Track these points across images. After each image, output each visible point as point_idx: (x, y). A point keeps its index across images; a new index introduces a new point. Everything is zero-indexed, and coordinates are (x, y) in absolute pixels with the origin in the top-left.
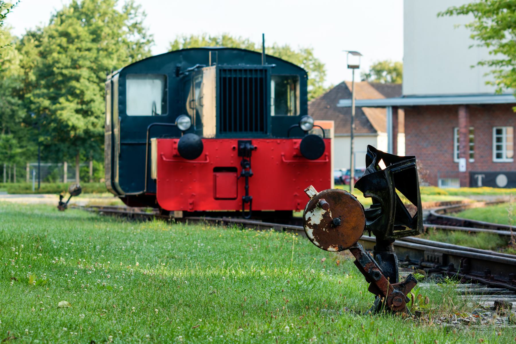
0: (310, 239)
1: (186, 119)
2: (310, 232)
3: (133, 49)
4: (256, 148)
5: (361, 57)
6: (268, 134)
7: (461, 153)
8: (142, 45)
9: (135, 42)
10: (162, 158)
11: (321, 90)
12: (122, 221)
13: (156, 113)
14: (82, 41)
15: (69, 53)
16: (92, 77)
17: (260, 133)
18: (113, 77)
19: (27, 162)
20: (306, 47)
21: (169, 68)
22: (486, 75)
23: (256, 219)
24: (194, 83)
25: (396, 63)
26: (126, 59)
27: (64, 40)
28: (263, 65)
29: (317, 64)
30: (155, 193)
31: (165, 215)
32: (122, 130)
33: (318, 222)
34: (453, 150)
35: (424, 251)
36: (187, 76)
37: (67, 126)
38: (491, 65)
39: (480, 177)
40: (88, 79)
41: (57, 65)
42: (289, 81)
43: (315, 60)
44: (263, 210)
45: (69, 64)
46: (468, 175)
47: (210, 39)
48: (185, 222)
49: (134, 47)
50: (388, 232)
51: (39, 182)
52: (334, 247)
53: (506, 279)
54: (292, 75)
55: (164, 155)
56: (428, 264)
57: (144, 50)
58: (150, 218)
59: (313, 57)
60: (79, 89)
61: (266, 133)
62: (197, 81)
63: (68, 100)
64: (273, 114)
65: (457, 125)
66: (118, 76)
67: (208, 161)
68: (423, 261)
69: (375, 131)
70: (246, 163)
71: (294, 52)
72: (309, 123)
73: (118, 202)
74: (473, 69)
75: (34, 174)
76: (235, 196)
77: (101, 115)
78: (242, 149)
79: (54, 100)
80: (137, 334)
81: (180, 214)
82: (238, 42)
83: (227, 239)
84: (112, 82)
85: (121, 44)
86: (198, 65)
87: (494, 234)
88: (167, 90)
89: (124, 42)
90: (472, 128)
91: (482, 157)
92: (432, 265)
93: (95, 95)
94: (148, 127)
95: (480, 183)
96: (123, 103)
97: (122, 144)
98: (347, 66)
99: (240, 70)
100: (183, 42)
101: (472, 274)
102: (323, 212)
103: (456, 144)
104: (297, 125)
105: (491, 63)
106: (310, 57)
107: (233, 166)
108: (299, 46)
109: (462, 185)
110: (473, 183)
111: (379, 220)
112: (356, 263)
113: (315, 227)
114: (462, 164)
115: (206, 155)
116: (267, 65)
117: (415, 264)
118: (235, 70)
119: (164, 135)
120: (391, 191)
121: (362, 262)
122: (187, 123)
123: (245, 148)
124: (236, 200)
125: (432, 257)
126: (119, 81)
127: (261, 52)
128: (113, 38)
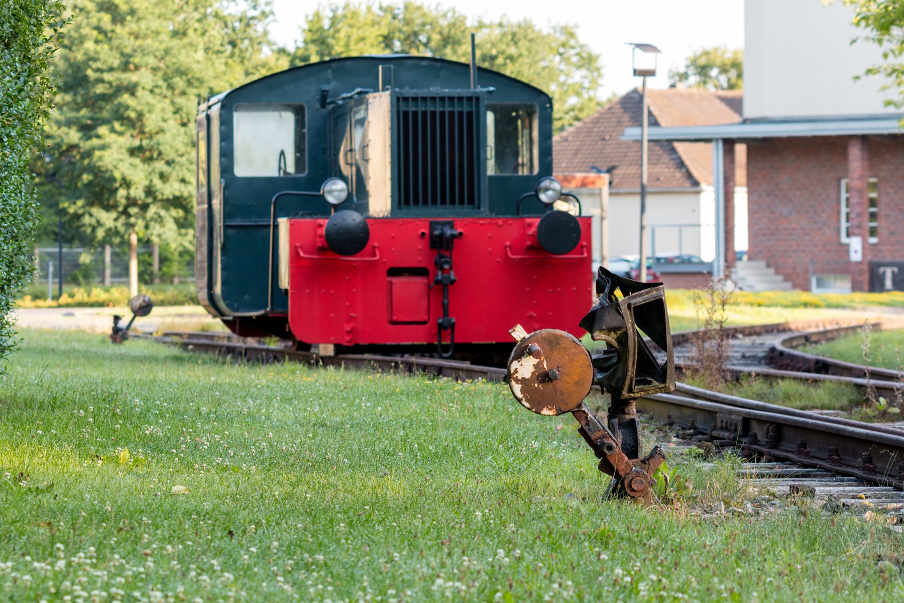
0: (516, 398)
1: (340, 185)
2: (517, 388)
3: (234, 30)
4: (461, 234)
5: (659, 54)
6: (482, 209)
7: (852, 227)
8: (252, 22)
9: (239, 15)
10: (298, 253)
11: (593, 104)
12: (224, 363)
13: (285, 172)
14: (139, 19)
15: (116, 43)
16: (160, 87)
17: (467, 208)
18: (209, 107)
19: (35, 245)
20: (563, 23)
21: (308, 93)
22: (884, 89)
23: (463, 359)
24: (353, 120)
25: (736, 52)
26: (221, 49)
27: (106, 18)
28: (472, 89)
29: (584, 55)
30: (287, 314)
31: (302, 352)
32: (226, 202)
33: (528, 375)
34: (838, 220)
35: (716, 413)
36: (340, 106)
37: (113, 179)
38: (890, 75)
39: (889, 272)
40: (152, 91)
41: (95, 65)
42: (521, 112)
43: (582, 46)
44: (474, 342)
45: (116, 63)
46: (865, 267)
47: (381, 8)
48: (340, 365)
49: (237, 24)
50: (626, 388)
51: (61, 284)
52: (550, 409)
53: (826, 455)
54: (526, 104)
55: (301, 248)
56: (722, 434)
57: (255, 30)
58: (276, 357)
59: (577, 42)
60: (134, 110)
61: (479, 208)
62: (358, 117)
63: (113, 130)
64: (491, 168)
65: (846, 174)
66: (219, 105)
67: (377, 258)
68: (715, 428)
69: (696, 183)
70: (443, 260)
71: (540, 31)
72: (553, 190)
73: (217, 326)
74: (858, 82)
75: (51, 269)
76: (426, 318)
77: (178, 159)
78: (436, 236)
79: (87, 130)
80: (286, 523)
81: (327, 350)
82: (434, 13)
83: (408, 395)
84: (208, 118)
85: (211, 19)
86: (359, 90)
87: (848, 384)
88: (305, 130)
89: (216, 16)
90: (873, 180)
91: (892, 233)
92: (727, 434)
93: (165, 121)
94: (273, 199)
95: (888, 284)
96: (227, 154)
97: (226, 227)
98: (632, 72)
99: (433, 99)
100: (331, 14)
101: (782, 448)
102: (536, 361)
103: (844, 210)
104: (533, 193)
105: (889, 70)
106: (572, 42)
107: (422, 265)
108: (549, 20)
109: (856, 287)
110: (875, 284)
111: (615, 371)
112: (582, 431)
113: (523, 381)
114: (856, 248)
115: (374, 248)
116: (479, 89)
117: (703, 434)
118: (424, 99)
119: (301, 213)
120: (630, 331)
121: (590, 430)
122: (340, 191)
123: (442, 235)
124: (428, 325)
125: (727, 422)
126: (221, 115)
127: (470, 62)
128: (196, 9)
